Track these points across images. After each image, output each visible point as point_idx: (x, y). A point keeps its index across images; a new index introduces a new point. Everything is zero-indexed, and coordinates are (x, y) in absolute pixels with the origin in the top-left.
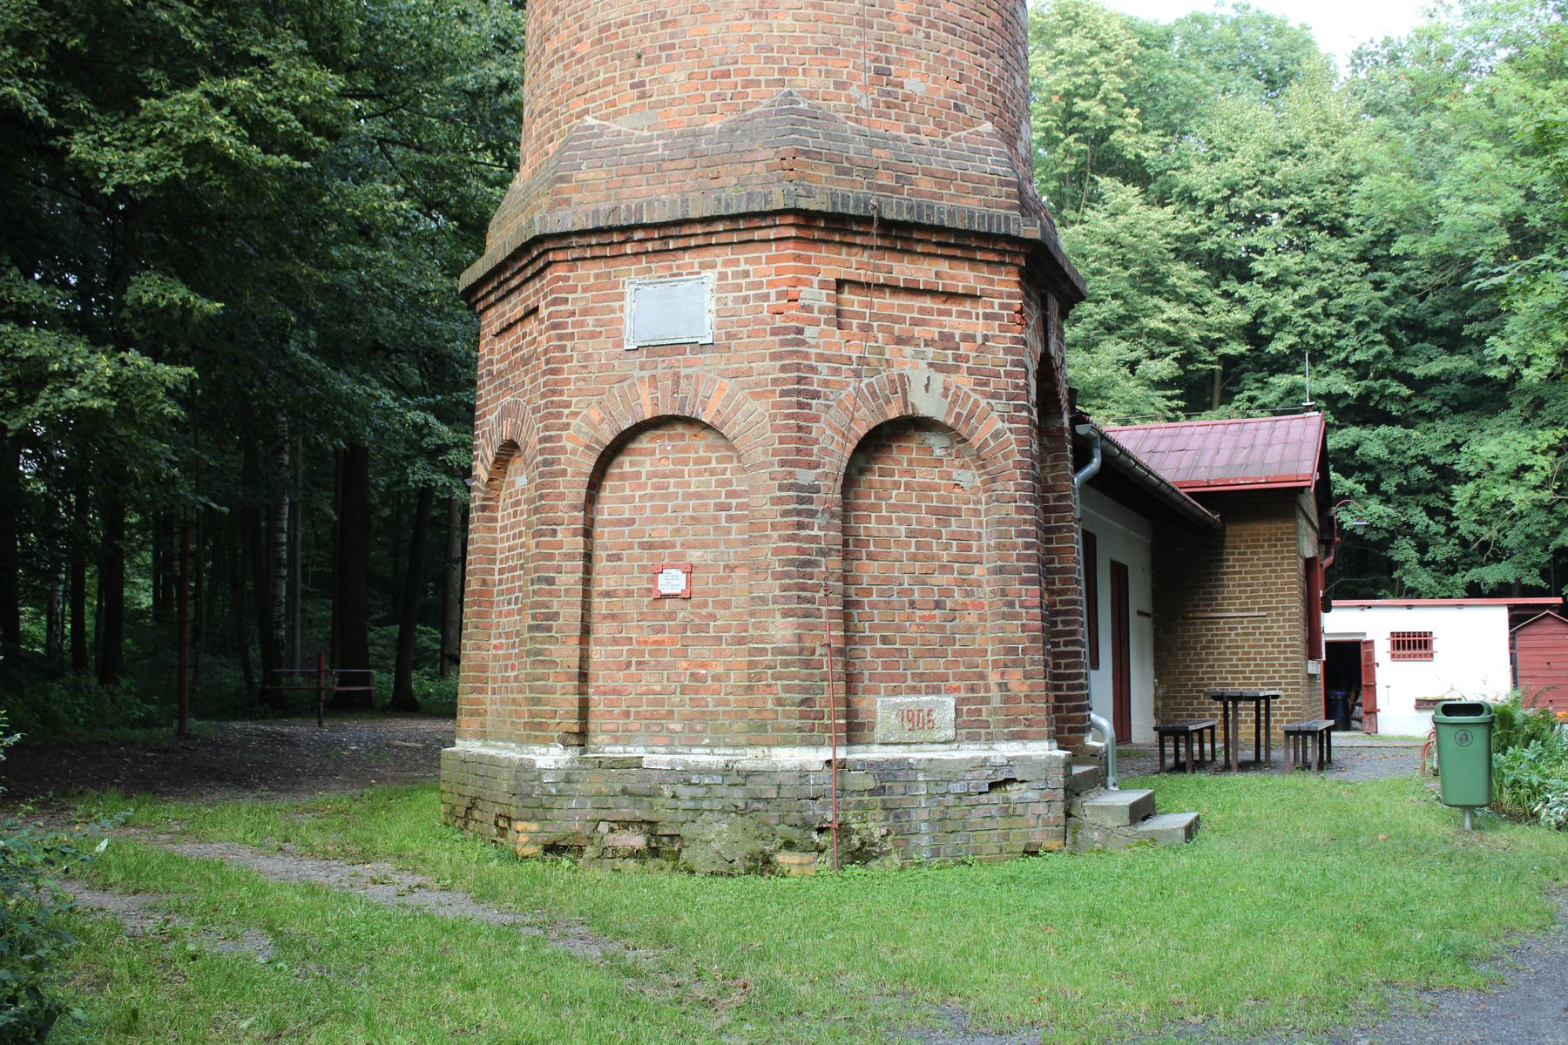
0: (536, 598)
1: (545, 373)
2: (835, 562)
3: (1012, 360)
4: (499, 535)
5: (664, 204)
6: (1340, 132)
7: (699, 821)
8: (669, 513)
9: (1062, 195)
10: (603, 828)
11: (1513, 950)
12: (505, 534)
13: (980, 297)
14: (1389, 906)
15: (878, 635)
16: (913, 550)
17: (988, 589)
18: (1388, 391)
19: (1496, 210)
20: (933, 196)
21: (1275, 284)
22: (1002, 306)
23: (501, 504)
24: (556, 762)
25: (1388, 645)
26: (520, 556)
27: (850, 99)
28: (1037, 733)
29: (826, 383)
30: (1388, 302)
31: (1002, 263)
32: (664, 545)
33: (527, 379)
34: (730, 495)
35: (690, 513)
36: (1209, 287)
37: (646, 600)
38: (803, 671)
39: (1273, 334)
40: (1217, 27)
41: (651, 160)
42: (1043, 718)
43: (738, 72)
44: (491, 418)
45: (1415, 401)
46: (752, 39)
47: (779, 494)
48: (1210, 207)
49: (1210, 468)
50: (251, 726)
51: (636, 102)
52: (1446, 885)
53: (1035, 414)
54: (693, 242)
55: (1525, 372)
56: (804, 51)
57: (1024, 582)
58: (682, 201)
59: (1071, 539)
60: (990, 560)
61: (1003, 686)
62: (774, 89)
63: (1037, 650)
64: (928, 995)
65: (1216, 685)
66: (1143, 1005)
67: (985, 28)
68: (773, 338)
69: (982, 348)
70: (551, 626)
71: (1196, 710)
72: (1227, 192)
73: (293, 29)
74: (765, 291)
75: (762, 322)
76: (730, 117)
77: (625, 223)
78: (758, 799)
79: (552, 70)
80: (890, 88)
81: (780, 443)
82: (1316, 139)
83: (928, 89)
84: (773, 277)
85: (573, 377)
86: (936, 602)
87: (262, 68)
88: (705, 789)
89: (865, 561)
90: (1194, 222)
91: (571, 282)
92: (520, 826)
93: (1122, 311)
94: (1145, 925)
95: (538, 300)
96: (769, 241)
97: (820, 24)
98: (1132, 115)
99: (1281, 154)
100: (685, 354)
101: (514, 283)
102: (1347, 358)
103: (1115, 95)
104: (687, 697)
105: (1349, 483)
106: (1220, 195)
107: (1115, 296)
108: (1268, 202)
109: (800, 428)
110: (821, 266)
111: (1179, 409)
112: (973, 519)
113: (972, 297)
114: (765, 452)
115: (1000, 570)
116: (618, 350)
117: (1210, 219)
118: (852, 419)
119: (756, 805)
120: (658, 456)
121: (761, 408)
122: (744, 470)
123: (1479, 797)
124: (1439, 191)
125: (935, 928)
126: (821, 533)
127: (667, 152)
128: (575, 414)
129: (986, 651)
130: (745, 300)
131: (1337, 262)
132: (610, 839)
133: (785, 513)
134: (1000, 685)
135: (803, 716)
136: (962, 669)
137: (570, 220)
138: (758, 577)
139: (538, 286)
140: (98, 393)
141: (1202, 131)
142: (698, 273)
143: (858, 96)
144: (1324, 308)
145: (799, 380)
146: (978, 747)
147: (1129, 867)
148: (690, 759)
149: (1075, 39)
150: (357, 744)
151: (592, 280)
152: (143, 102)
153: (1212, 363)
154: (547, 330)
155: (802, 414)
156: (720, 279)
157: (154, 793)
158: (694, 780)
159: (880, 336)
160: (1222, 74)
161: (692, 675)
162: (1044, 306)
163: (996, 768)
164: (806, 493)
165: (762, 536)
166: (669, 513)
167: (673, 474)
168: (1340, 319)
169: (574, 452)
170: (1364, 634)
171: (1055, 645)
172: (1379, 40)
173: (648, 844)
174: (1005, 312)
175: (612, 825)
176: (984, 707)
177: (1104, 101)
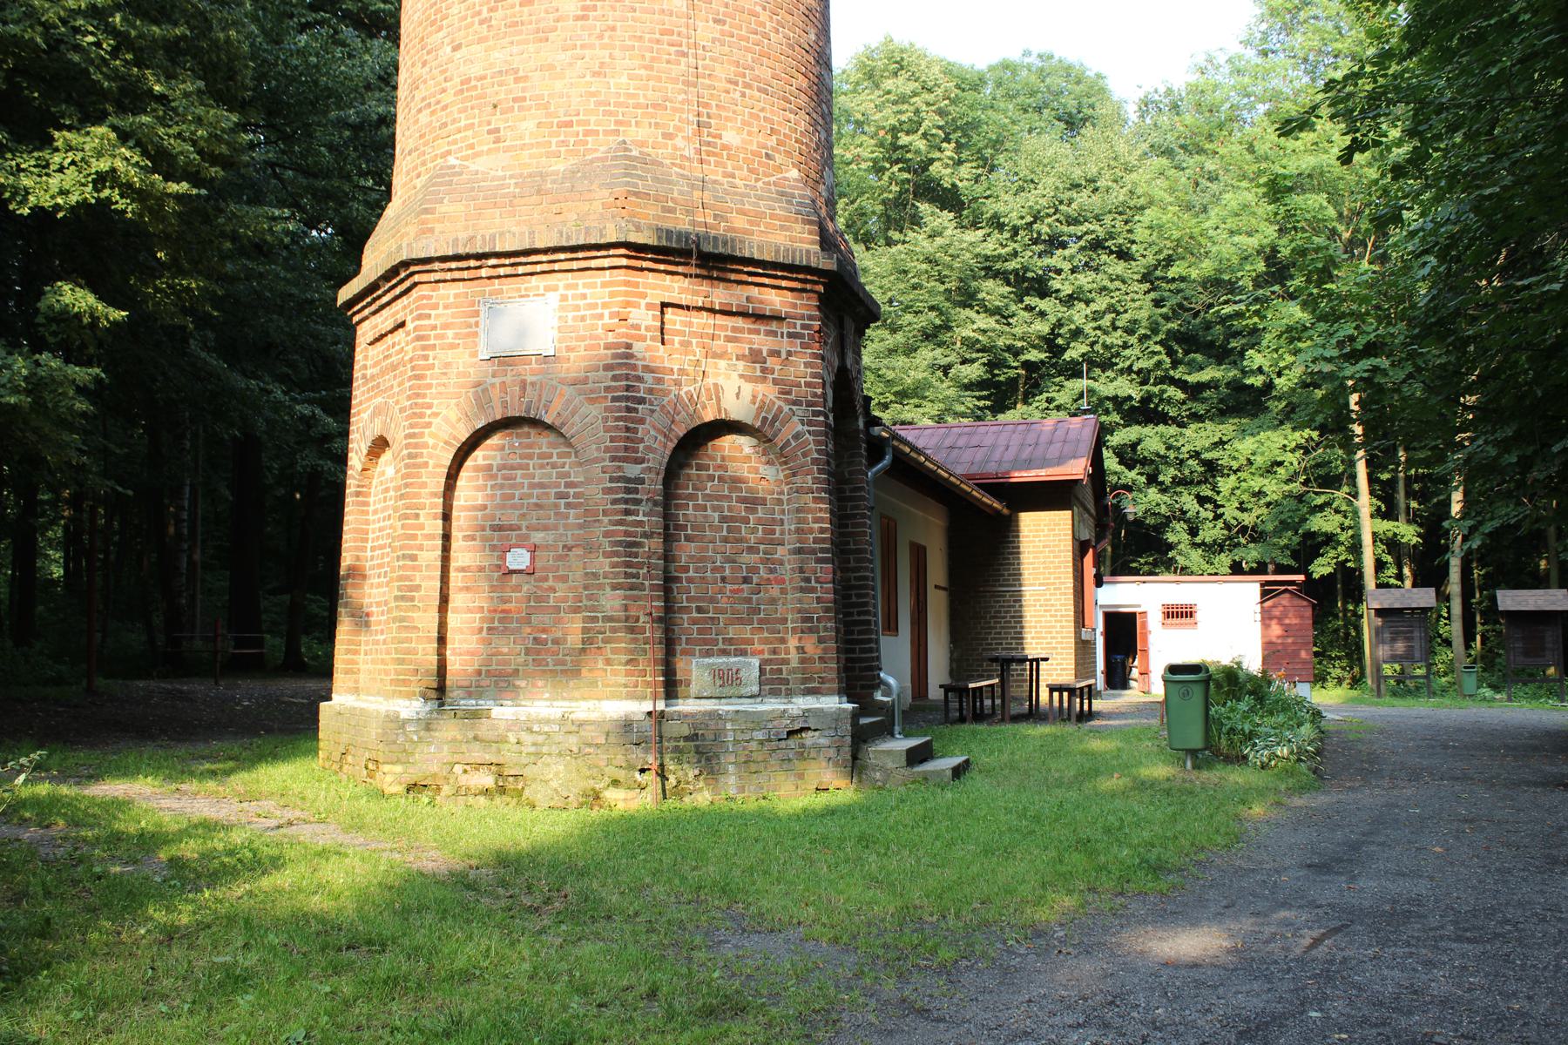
1: (410, 379)
2: (656, 544)
4: (371, 517)
6: (1128, 169)
8: (516, 500)
9: (888, 217)
10: (458, 769)
11: (1199, 863)
14: (1108, 830)
16: (725, 533)
18: (1165, 396)
19: (1253, 242)
20: (746, 232)
21: (1070, 301)
22: (804, 327)
23: (372, 490)
24: (418, 713)
25: (1161, 616)
27: (675, 148)
29: (651, 391)
30: (1167, 318)
31: (803, 290)
32: (511, 528)
33: (395, 383)
34: (568, 485)
35: (534, 501)
39: (1068, 344)
40: (1024, 73)
41: (504, 196)
42: (834, 675)
43: (579, 123)
44: (365, 416)
45: (1190, 404)
46: (593, 94)
47: (609, 485)
48: (1015, 231)
49: (1000, 462)
50: (153, 684)
52: (1159, 814)
54: (539, 268)
55: (1277, 381)
56: (637, 106)
57: (819, 561)
59: (864, 525)
60: (791, 542)
61: (801, 650)
63: (829, 619)
64: (716, 902)
65: (1003, 649)
66: (891, 910)
67: (793, 88)
71: (986, 671)
72: (1029, 219)
73: (192, 70)
74: (599, 311)
75: (597, 337)
77: (480, 251)
78: (590, 745)
79: (420, 116)
80: (710, 139)
82: (1107, 174)
83: (744, 141)
84: (607, 299)
85: (434, 382)
87: (164, 105)
88: (544, 737)
89: (683, 542)
90: (1001, 244)
92: (386, 768)
93: (938, 322)
94: (905, 846)
96: (603, 269)
97: (651, 83)
98: (949, 150)
99: (1075, 186)
102: (1131, 366)
103: (934, 131)
105: (1132, 474)
107: (932, 308)
108: (1065, 229)
109: (628, 429)
110: (649, 291)
111: (987, 408)
113: (777, 318)
114: (598, 449)
115: (799, 551)
116: (474, 360)
118: (673, 422)
122: (581, 464)
123: (1197, 742)
124: (1207, 224)
125: (731, 850)
126: (645, 519)
127: (517, 190)
128: (436, 415)
130: (583, 319)
131: (1124, 282)
132: (464, 780)
133: (615, 502)
134: (797, 648)
135: (628, 674)
136: (766, 635)
138: (592, 556)
140: (16, 390)
144: (1113, 323)
145: (628, 388)
147: (903, 801)
149: (900, 80)
151: (452, 300)
152: (57, 134)
153: (1016, 368)
154: (413, 341)
157: (65, 742)
158: (536, 728)
161: (535, 639)
162: (841, 326)
163: (793, 719)
164: (632, 485)
166: (516, 500)
167: (520, 467)
168: (1126, 332)
169: (435, 447)
170: (1139, 606)
172: (1162, 90)
176: (784, 667)
177: (925, 135)
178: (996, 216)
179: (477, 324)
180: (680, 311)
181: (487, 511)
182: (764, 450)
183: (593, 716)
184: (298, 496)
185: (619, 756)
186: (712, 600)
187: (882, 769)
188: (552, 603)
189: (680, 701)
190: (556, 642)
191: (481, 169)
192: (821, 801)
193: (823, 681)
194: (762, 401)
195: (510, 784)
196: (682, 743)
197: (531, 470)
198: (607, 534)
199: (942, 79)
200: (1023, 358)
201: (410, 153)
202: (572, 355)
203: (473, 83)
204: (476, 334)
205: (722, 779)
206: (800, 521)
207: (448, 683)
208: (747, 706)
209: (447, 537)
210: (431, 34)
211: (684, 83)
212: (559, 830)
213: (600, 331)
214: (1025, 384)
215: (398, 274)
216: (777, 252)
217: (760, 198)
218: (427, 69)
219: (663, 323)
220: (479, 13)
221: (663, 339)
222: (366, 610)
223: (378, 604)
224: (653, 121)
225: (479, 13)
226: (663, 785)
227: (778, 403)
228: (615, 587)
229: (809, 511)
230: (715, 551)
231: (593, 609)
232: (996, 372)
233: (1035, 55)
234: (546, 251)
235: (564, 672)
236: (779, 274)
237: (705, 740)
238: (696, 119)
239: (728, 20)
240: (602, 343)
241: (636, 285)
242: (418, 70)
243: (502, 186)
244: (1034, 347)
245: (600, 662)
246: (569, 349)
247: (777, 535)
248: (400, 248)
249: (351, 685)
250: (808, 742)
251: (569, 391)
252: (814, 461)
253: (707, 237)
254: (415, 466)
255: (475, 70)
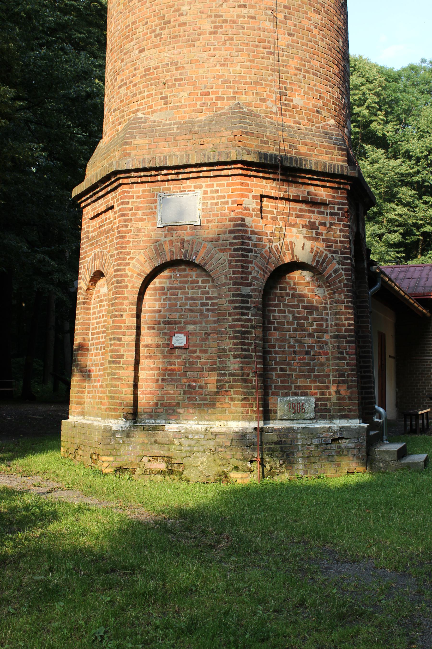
0: (112, 348)
1: (117, 238)
3: (343, 235)
4: (91, 316)
5: (177, 156)
7: (192, 457)
10: (145, 459)
12: (95, 316)
13: (329, 204)
15: (279, 367)
16: (295, 326)
17: (330, 346)
20: (307, 155)
22: (339, 209)
23: (92, 301)
26: (103, 327)
27: (267, 107)
28: (354, 415)
29: (255, 245)
31: (339, 188)
32: (175, 323)
33: (108, 241)
34: (208, 298)
36: (417, 199)
37: (166, 349)
38: (244, 384)
40: (422, 72)
41: (171, 135)
42: (356, 408)
43: (213, 93)
44: (89, 259)
46: (220, 77)
47: (232, 298)
48: (418, 160)
49: (424, 287)
51: (163, 106)
53: (354, 261)
54: (191, 175)
57: (348, 342)
58: (186, 156)
61: (337, 393)
62: (231, 102)
63: (354, 375)
67: (331, 73)
68: (230, 223)
69: (329, 229)
70: (120, 361)
72: (426, 153)
74: (226, 200)
75: (225, 215)
76: (209, 114)
77: (158, 166)
78: (221, 446)
79: (120, 90)
80: (286, 102)
81: (233, 274)
83: (305, 103)
84: (230, 193)
85: (131, 240)
86: (306, 351)
88: (195, 441)
89: (273, 331)
90: (410, 167)
91: (131, 194)
92: (104, 458)
95: (114, 202)
96: (228, 176)
97: (253, 70)
98: (381, 115)
100: (187, 230)
101: (101, 194)
103: (373, 105)
104: (186, 396)
106: (423, 154)
109: (243, 267)
110: (254, 188)
112: (324, 312)
113: (324, 204)
114: (226, 278)
116: (154, 227)
117: (418, 166)
119: (220, 449)
120: (173, 279)
121: (224, 257)
122: (215, 287)
127: (178, 131)
128: (132, 258)
129: (329, 375)
130: (217, 204)
132: (149, 466)
133: (235, 308)
134: (336, 392)
136: (318, 384)
137: (131, 163)
138: (222, 339)
139: (114, 195)
141: (414, 123)
142: (193, 191)
143: (271, 106)
146: (325, 421)
147: (399, 480)
148: (188, 426)
150: (11, 417)
151: (141, 193)
153: (418, 235)
154: (119, 217)
155: (244, 260)
156: (204, 194)
158: (190, 437)
159: (281, 222)
160: (424, 95)
161: (189, 385)
163: (335, 432)
165: (224, 319)
166: (178, 307)
167: (180, 288)
169: (132, 277)
171: (361, 372)
173: (167, 468)
174: (340, 212)
175: (150, 458)
176: (328, 403)
177: (368, 107)
178: (407, 152)
179: (156, 207)
180: (271, 200)
181: (161, 313)
182: (317, 279)
183: (223, 430)
184: (24, 305)
185: (239, 453)
186: (289, 364)
187: (384, 461)
188: (198, 366)
189: (271, 422)
190: (201, 387)
191: (157, 119)
192: (352, 479)
193: (350, 410)
194: (316, 251)
195: (175, 468)
196: (273, 446)
197: (187, 290)
198: (231, 326)
199: (378, 76)
200: (423, 230)
201: (114, 111)
202: (211, 225)
203: (151, 71)
204: (155, 213)
205: (295, 466)
206: (337, 319)
207: (139, 410)
208: (308, 425)
209: (138, 328)
210: (126, 43)
211: (272, 70)
212: (210, 495)
213: (226, 211)
214: (422, 245)
215: (110, 179)
216: (325, 166)
217: (314, 136)
218: (124, 63)
219: (261, 207)
220: (155, 31)
221: (262, 216)
222: (88, 368)
223: (96, 365)
224: (255, 91)
225: (155, 31)
226: (263, 470)
227: (325, 252)
228: (235, 357)
229: (343, 314)
230: (290, 336)
231: (223, 369)
232: (408, 238)
233: (428, 62)
234: (195, 166)
235: (205, 404)
236: (326, 179)
237: (286, 444)
238: (278, 90)
239: (296, 34)
240: (228, 218)
241: (247, 185)
242: (118, 64)
243: (169, 129)
244: (428, 224)
245: (227, 399)
246: (209, 221)
247: (324, 327)
248: (112, 164)
249: (80, 410)
250: (343, 446)
251: (208, 245)
252: (345, 286)
253: (286, 157)
254: (121, 287)
255: (153, 63)
